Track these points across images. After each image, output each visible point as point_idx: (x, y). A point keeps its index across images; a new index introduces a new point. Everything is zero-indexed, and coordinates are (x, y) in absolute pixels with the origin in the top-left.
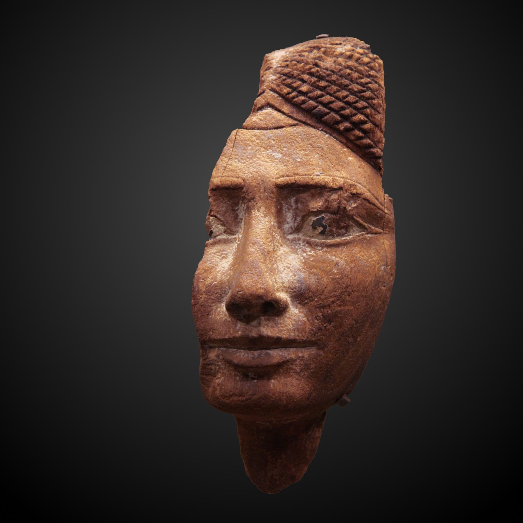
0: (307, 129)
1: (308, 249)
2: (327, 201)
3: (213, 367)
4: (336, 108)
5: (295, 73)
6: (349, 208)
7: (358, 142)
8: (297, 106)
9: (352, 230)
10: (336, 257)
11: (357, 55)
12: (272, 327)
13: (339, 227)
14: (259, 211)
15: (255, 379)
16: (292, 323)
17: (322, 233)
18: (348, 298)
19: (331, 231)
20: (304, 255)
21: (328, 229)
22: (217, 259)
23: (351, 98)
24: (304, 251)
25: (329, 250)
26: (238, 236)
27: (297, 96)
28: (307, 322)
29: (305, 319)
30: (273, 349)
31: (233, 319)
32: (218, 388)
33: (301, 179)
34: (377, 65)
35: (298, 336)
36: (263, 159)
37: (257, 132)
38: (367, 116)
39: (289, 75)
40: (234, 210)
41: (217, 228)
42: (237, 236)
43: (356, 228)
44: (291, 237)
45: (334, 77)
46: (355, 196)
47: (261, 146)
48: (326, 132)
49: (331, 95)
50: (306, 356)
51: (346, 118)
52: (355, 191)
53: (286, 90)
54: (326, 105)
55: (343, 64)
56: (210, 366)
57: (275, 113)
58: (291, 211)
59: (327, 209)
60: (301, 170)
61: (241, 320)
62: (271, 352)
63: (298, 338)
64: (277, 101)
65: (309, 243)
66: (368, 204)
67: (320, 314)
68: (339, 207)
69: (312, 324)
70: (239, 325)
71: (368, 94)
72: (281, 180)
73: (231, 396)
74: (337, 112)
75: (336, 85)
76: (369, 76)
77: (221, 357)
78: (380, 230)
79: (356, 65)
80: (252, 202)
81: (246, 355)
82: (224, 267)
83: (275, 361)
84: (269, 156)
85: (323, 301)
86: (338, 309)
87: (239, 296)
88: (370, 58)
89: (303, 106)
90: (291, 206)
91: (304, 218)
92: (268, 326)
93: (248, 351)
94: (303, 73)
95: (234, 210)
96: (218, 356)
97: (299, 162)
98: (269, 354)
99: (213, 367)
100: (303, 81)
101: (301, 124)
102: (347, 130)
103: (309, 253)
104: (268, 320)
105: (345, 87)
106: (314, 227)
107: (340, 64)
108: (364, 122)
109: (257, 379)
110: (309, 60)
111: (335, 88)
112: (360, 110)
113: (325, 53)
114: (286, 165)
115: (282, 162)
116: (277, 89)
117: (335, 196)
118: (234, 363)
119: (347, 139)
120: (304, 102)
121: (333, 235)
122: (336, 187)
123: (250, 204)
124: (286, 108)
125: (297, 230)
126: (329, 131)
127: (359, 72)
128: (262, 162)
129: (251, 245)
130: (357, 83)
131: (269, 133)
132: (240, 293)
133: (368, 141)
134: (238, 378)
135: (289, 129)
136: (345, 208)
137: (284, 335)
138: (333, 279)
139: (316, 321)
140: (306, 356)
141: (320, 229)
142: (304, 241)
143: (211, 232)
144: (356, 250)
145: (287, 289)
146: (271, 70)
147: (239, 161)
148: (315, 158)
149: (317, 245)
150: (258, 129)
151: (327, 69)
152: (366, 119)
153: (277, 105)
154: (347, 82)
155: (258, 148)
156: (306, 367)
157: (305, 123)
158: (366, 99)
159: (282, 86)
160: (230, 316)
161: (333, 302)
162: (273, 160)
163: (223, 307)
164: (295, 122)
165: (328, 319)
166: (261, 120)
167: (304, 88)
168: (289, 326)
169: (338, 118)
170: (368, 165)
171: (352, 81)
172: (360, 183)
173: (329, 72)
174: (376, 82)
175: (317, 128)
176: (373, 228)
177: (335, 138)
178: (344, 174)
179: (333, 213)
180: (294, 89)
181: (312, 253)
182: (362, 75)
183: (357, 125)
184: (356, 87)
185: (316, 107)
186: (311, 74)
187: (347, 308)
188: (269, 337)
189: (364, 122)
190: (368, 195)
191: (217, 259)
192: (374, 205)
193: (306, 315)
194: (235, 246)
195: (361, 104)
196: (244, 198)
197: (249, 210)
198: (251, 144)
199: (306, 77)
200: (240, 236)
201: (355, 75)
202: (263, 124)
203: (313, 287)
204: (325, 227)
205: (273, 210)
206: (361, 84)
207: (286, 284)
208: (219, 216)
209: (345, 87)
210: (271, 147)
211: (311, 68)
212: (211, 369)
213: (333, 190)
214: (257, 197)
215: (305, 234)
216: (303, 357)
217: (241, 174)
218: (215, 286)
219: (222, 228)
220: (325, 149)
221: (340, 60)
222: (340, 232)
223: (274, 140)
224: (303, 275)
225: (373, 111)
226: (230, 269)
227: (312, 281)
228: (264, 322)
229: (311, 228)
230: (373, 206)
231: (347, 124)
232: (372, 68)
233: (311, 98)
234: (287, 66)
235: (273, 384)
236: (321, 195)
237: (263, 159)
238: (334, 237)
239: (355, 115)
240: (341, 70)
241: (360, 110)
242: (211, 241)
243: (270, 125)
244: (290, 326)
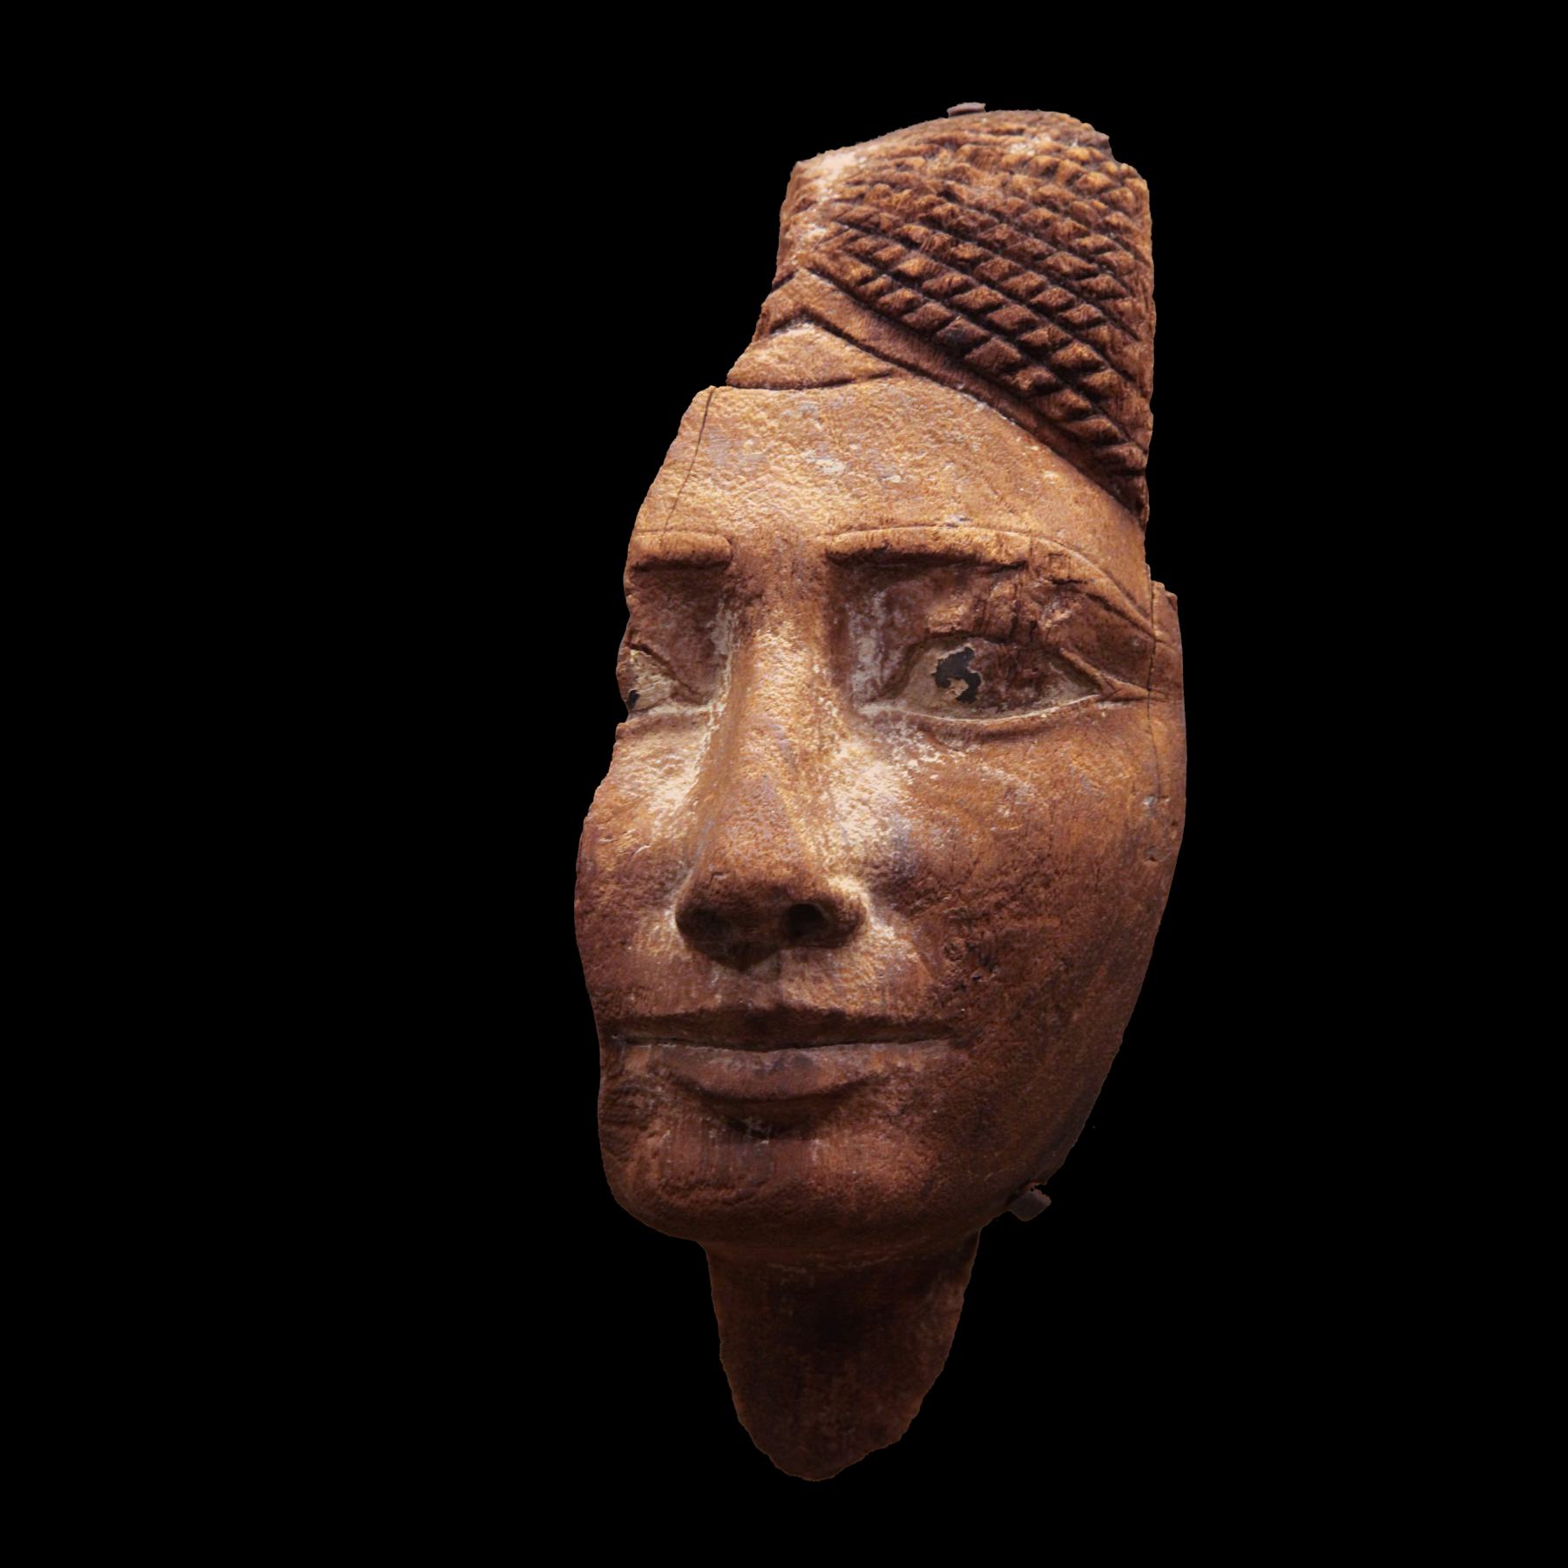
0: (920, 386)
1: (923, 747)
2: (979, 602)
3: (638, 1100)
4: (1007, 324)
5: (886, 217)
6: (1046, 624)
7: (1073, 427)
8: (891, 318)
9: (1054, 691)
10: (1007, 770)
11: (1070, 166)
12: (817, 980)
13: (1017, 682)
14: (776, 634)
15: (763, 1137)
16: (875, 969)
17: (967, 699)
18: (1042, 894)
19: (992, 692)
20: (913, 763)
21: (982, 686)
22: (650, 776)
23: (1054, 295)
24: (912, 754)
25: (986, 749)
26: (715, 707)
28: (921, 965)
29: (914, 956)
30: (819, 1045)
31: (699, 958)
32: (654, 1163)
33: (902, 536)
34: (1130, 194)
35: (895, 1007)
36: (787, 476)
37: (770, 395)
38: (1099, 346)
39: (866, 226)
40: (701, 631)
42: (709, 708)
43: (1067, 685)
44: (871, 710)
45: (1001, 232)
46: (1065, 587)
48: (978, 396)
49: (992, 284)
50: (918, 1067)
51: (1037, 354)
52: (1063, 574)
53: (857, 270)
54: (976, 315)
55: (1029, 190)
56: (630, 1099)
57: (825, 339)
58: (873, 632)
59: (979, 627)
60: (901, 511)
61: (722, 960)
62: (813, 1055)
63: (892, 1013)
64: (832, 304)
65: (926, 729)
66: (1103, 612)
67: (959, 941)
68: (1015, 621)
69: (936, 971)
70: (718, 974)
71: (1103, 281)
72: (844, 541)
73: (692, 1187)
74: (1009, 335)
75: (1006, 254)
76: (1106, 228)
77: (662, 1071)
78: (1140, 691)
79: (1069, 194)
80: (757, 605)
81: (739, 1064)
83: (824, 1082)
84: (807, 468)
85: (967, 901)
87: (717, 886)
88: (1108, 173)
89: (910, 318)
90: (873, 618)
91: (912, 654)
92: (803, 978)
93: (744, 1053)
94: (909, 218)
95: (701, 631)
96: (652, 1068)
97: (897, 486)
98: (806, 1062)
99: (638, 1100)
100: (910, 243)
101: (904, 371)
102: (1041, 389)
103: (926, 759)
104: (805, 959)
105: (1034, 261)
106: (942, 682)
107: (1019, 193)
108: (1092, 367)
109: (772, 1136)
111: (1004, 263)
112: (1079, 331)
113: (973, 158)
114: (856, 496)
115: (847, 485)
116: (831, 266)
117: (1003, 589)
118: (702, 1089)
119: (1042, 417)
120: (911, 306)
121: (997, 704)
122: (1007, 562)
123: (751, 612)
124: (858, 325)
125: (891, 689)
126: (985, 393)
127: (1077, 214)
128: (784, 487)
129: (753, 734)
130: (1071, 250)
131: (806, 398)
132: (720, 878)
133: (1102, 423)
134: (712, 1134)
135: (868, 387)
137: (853, 1004)
138: (997, 837)
139: (947, 962)
140: (918, 1067)
141: (960, 687)
142: (911, 722)
144: (1067, 749)
145: (861, 868)
146: (814, 211)
147: (716, 481)
148: (943, 474)
149: (951, 735)
150: (774, 387)
151: (980, 207)
152: (1098, 358)
153: (831, 315)
154: (1041, 246)
156: (918, 1101)
157: (915, 370)
158: (1098, 297)
159: (846, 259)
160: (689, 948)
161: (999, 906)
162: (818, 478)
164: (884, 366)
165: (983, 957)
166: (781, 360)
167: (913, 264)
168: (866, 979)
169: (1014, 353)
170: (1104, 494)
171: (1054, 242)
172: (1078, 550)
173: (986, 217)
175: (952, 385)
176: (1118, 683)
177: (1004, 415)
178: (1030, 521)
179: (1000, 639)
180: (882, 267)
181: (937, 758)
182: (1086, 224)
183: (1072, 375)
184: (1067, 262)
186: (934, 223)
187: (1039, 923)
188: (806, 1012)
189: (1092, 367)
190: (1103, 583)
191: (650, 776)
192: (1122, 614)
193: (917, 945)
195: (1083, 311)
196: (732, 594)
197: (745, 629)
198: (752, 432)
199: (917, 230)
200: (721, 708)
201: (1066, 225)
202: (787, 371)
203: (939, 861)
204: (973, 681)
205: (819, 629)
206: (1083, 253)
207: (859, 853)
208: (655, 648)
209: (1034, 261)
210: (813, 440)
211: (932, 205)
213: (998, 570)
214: (770, 591)
215: (914, 703)
216: (909, 1069)
217: (722, 523)
218: (646, 857)
219: (665, 684)
221: (1020, 179)
222: (1020, 694)
223: (820, 420)
224: (908, 825)
225: (1118, 332)
226: (690, 807)
227: (936, 841)
228: (790, 967)
229: (932, 683)
230: (1117, 619)
231: (1042, 373)
232: (1114, 205)
233: (931, 295)
235: (820, 1152)
236: (962, 583)
237: (787, 476)
238: (1000, 711)
239: (1065, 344)
240: (1021, 210)
241: (1079, 331)
243: (810, 375)
244: (869, 977)
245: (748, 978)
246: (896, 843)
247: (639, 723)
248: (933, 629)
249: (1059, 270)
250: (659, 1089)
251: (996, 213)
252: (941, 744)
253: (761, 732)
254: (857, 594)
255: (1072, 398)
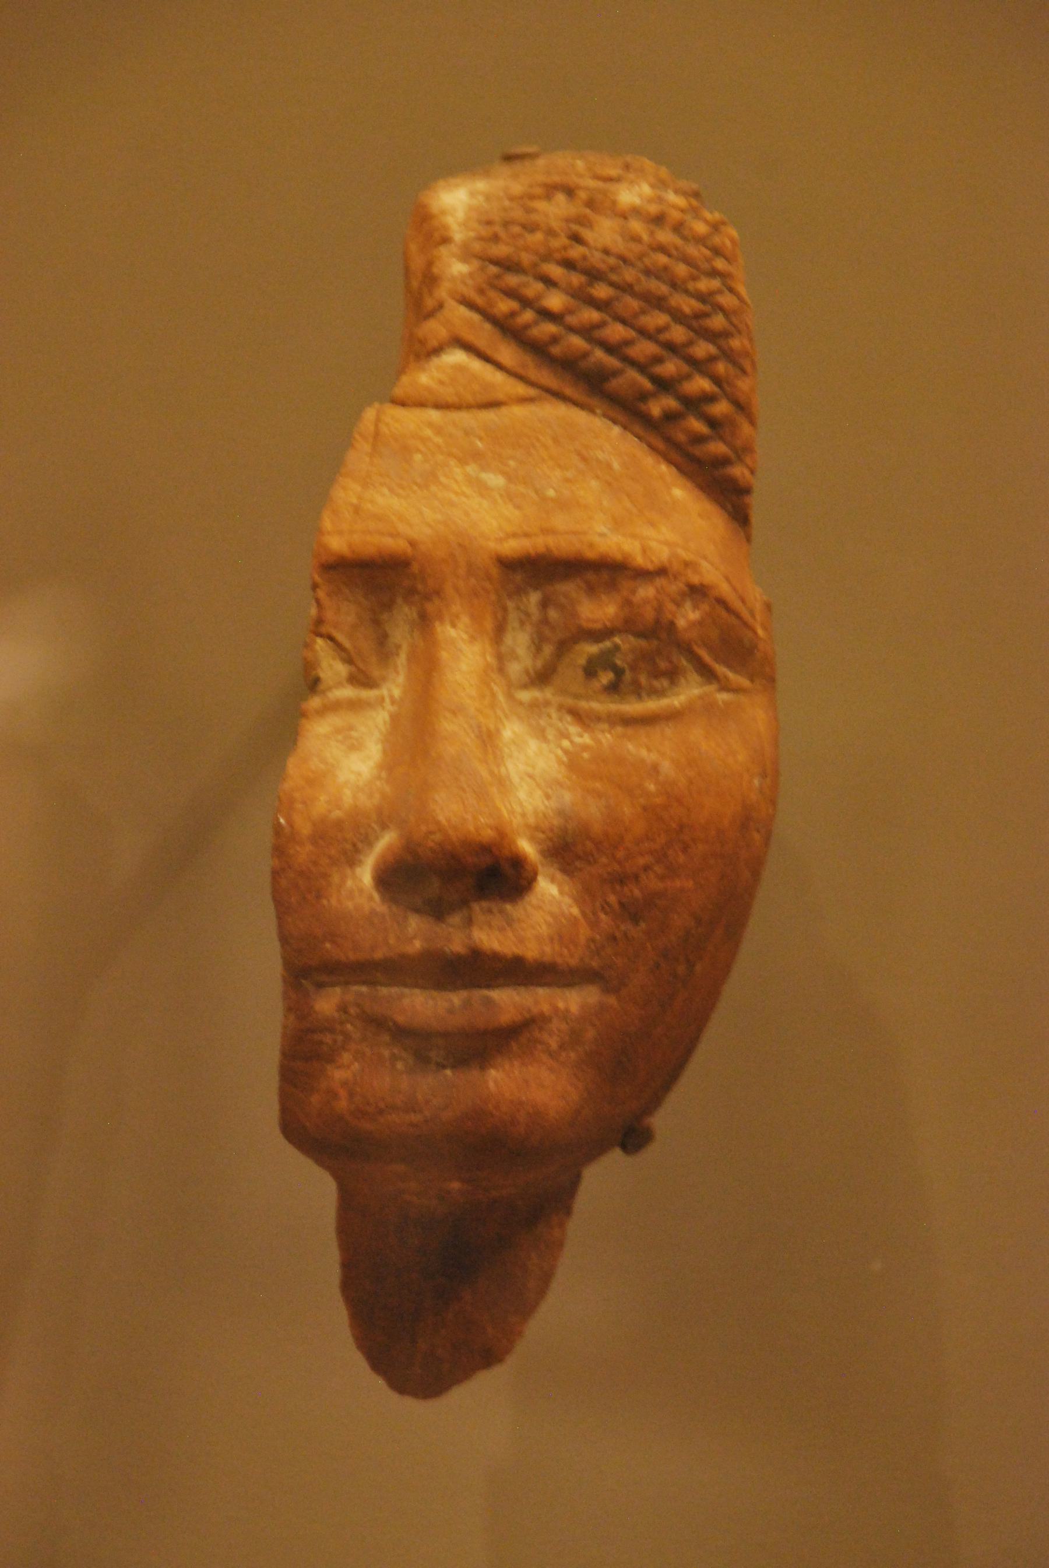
0: (562, 410)
1: (573, 729)
2: (628, 603)
3: (328, 1038)
4: (642, 359)
5: (526, 258)
6: (681, 623)
7: (697, 451)
8: (538, 349)
9: (683, 681)
10: (649, 750)
11: (675, 215)
12: (501, 929)
13: (657, 674)
14: (454, 626)
15: (444, 1067)
16: (545, 920)
17: (613, 689)
18: (682, 858)
19: (636, 683)
20: (566, 743)
21: (628, 676)
22: (334, 751)
23: (678, 334)
24: (564, 735)
25: (630, 731)
26: (389, 690)
27: (536, 323)
28: (582, 921)
29: (575, 911)
30: (498, 986)
31: (394, 908)
32: (343, 1093)
33: (562, 545)
34: (728, 243)
35: (561, 955)
36: (455, 486)
37: (434, 415)
38: (717, 380)
39: (509, 265)
40: (376, 622)
41: (314, 672)
42: (384, 692)
43: (694, 677)
44: (525, 696)
45: (629, 275)
46: (697, 592)
47: (450, 455)
48: (615, 422)
49: (624, 322)
50: (574, 1008)
51: (664, 385)
52: (695, 580)
53: (504, 306)
54: (610, 349)
55: (645, 237)
56: (317, 1037)
57: (476, 365)
58: (528, 628)
59: (629, 625)
60: (560, 521)
61: (417, 910)
62: (496, 994)
63: (559, 960)
64: (484, 335)
65: (577, 715)
66: (724, 614)
67: (612, 899)
68: (657, 621)
69: (594, 924)
70: (414, 923)
71: (718, 322)
72: (512, 547)
73: (381, 1112)
74: (641, 368)
75: (635, 295)
76: (714, 273)
77: (353, 1011)
78: (745, 682)
79: (678, 241)
80: (437, 601)
81: (431, 1002)
82: (359, 774)
83: (507, 1017)
84: (471, 481)
85: (619, 863)
86: (660, 885)
87: (431, 844)
88: (706, 221)
89: (556, 350)
90: (528, 615)
91: (563, 647)
92: (490, 926)
93: (435, 993)
94: (547, 257)
95: (376, 622)
96: (343, 1008)
97: (552, 500)
98: (489, 1002)
99: (328, 1038)
100: (549, 282)
101: (548, 396)
102: (670, 417)
103: (578, 740)
104: (490, 911)
105: (658, 303)
106: (590, 671)
107: (636, 239)
108: (711, 399)
109: (453, 1067)
110: (555, 225)
111: (634, 304)
112: (698, 365)
113: (590, 204)
114: (518, 507)
115: (509, 497)
116: (479, 301)
117: (646, 592)
118: (395, 1023)
119: (668, 440)
120: (555, 340)
121: (638, 691)
122: (650, 567)
123: (430, 607)
124: (508, 353)
125: (542, 678)
126: (621, 418)
127: (687, 260)
128: (453, 497)
129: (448, 715)
130: (686, 292)
131: (465, 418)
132: (433, 837)
133: (717, 448)
134: (400, 1065)
135: (518, 411)
136: (672, 624)
137: (531, 952)
138: (645, 809)
139: (603, 916)
140: (574, 1008)
141: (606, 678)
142: (560, 707)
143: (317, 680)
144: (696, 733)
145: (534, 831)
146: (453, 248)
147: (391, 490)
148: (590, 489)
149: (599, 719)
150: (439, 406)
151: (606, 252)
152: (716, 389)
153: (481, 343)
154: (664, 289)
155: (440, 458)
156: (574, 1038)
157: (558, 395)
158: (712, 336)
159: (492, 294)
160: (384, 899)
161: (646, 868)
162: (483, 489)
163: (365, 875)
164: (532, 392)
165: (631, 912)
166: (441, 383)
167: (555, 301)
168: (539, 929)
169: (647, 384)
170: (724, 511)
171: (674, 285)
172: (705, 558)
173: (612, 261)
174: (731, 290)
175: (591, 410)
176: (731, 675)
177: (636, 437)
178: (666, 532)
179: (640, 635)
180: (526, 303)
181: (587, 739)
182: (698, 270)
183: (694, 404)
184: (688, 305)
185: (585, 355)
186: (569, 264)
187: (678, 883)
188: (496, 957)
189: (711, 399)
190: (724, 589)
191: (334, 751)
192: (738, 616)
193: (579, 901)
194: (381, 717)
195: (702, 349)
196: (412, 591)
197: (424, 622)
198: (421, 447)
199: (555, 271)
200: (397, 692)
201: (681, 270)
202: (448, 394)
203: (597, 829)
204: (619, 672)
205: (489, 624)
206: (702, 297)
207: (532, 820)
208: (340, 637)
209: (658, 303)
210: (476, 456)
211: (565, 248)
212: (321, 1043)
213: (643, 575)
214: (449, 590)
215: (563, 691)
216: (567, 1010)
217: (402, 527)
218: (339, 824)
219: (342, 669)
220: (616, 466)
221: (637, 226)
222: (656, 684)
223: (481, 439)
224: (567, 797)
225: (730, 366)
226: (379, 778)
227: (593, 811)
228: (479, 916)
229: (580, 673)
230: (733, 620)
231: (671, 403)
232: (717, 252)
233: (571, 329)
234: (495, 238)
235: (496, 1082)
236: (612, 586)
237: (455, 486)
238: (639, 697)
239: (688, 377)
240: (641, 257)
241: (698, 365)
242: (315, 702)
243: (469, 398)
244: (541, 927)
245: (444, 926)
246: (560, 813)
247: (701, 697)
248: (584, 624)
249: (681, 311)
250: (349, 1026)
251: (624, 260)
252: (589, 726)
253: (454, 713)
254: (519, 591)
255: (697, 425)
